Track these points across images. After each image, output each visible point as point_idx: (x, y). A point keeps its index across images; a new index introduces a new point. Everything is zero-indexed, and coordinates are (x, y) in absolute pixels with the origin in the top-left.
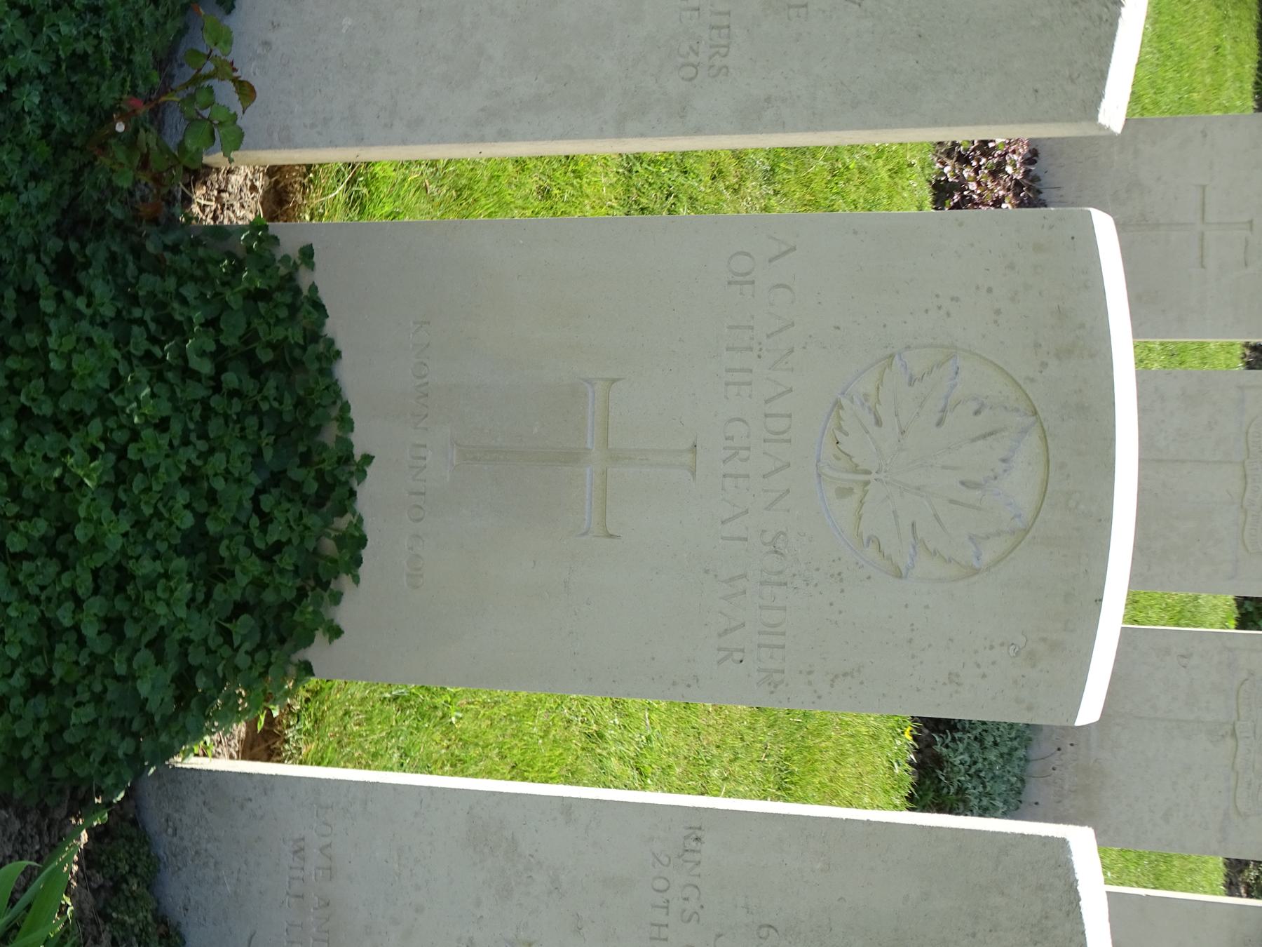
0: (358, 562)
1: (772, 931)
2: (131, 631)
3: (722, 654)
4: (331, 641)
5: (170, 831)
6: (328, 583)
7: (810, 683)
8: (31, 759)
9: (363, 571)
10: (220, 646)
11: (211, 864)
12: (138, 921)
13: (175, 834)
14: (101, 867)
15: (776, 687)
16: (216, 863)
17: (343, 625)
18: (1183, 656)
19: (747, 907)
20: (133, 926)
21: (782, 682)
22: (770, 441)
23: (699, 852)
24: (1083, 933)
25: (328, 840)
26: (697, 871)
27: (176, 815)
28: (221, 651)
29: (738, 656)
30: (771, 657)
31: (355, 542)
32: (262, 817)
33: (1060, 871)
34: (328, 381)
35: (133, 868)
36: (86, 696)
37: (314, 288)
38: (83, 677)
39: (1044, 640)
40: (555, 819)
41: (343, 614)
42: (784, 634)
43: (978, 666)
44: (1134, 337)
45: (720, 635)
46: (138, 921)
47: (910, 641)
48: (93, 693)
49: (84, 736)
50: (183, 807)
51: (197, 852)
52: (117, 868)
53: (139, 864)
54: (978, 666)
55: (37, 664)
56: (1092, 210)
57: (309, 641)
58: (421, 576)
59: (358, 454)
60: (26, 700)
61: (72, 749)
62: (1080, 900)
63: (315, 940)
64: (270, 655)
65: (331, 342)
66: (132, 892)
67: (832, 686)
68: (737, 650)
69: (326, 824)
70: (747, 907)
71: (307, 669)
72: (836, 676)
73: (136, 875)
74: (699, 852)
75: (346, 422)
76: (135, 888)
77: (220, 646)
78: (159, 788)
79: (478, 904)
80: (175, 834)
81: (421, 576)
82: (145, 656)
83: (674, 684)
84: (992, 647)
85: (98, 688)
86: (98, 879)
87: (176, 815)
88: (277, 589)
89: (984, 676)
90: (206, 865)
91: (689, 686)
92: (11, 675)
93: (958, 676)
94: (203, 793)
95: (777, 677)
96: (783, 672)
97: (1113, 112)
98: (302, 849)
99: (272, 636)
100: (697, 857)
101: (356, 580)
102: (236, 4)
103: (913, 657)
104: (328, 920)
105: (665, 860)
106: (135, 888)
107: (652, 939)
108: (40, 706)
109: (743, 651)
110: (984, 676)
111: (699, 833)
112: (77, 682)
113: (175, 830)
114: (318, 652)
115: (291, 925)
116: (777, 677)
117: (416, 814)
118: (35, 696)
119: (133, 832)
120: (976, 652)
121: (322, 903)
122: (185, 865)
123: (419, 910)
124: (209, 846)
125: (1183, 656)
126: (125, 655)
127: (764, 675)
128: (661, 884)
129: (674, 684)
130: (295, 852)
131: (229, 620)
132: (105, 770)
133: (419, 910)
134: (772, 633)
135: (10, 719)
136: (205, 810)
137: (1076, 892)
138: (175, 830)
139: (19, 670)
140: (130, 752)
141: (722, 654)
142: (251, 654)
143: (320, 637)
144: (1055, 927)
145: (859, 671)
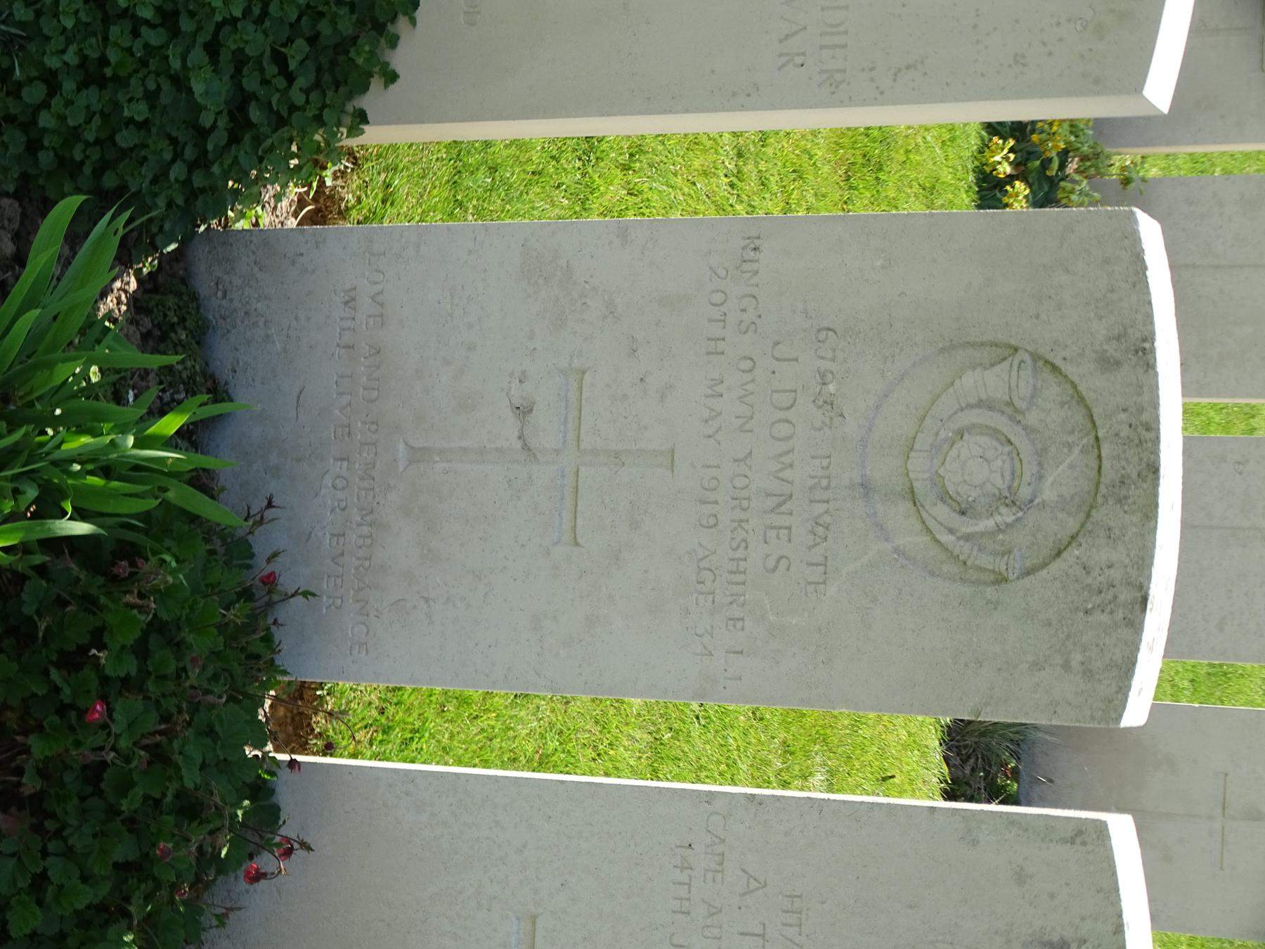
1: (831, 333)
2: (186, 25)
3: (784, 59)
4: (386, 86)
5: (220, 294)
6: (384, 25)
7: (872, 80)
8: (82, 163)
9: (420, 14)
10: (274, 76)
11: (261, 324)
12: (186, 368)
13: (224, 296)
14: (149, 312)
15: (837, 87)
16: (266, 322)
17: (399, 71)
18: (1239, 463)
19: (806, 312)
20: (180, 372)
21: (843, 81)
22: (827, 34)
23: (757, 261)
24: (1150, 303)
25: (378, 288)
26: (755, 280)
27: (226, 277)
28: (274, 81)
29: (798, 60)
30: (833, 58)
32: (313, 272)
33: (1126, 243)
35: (183, 320)
36: (139, 93)
38: (136, 71)
39: (1112, 11)
40: (611, 242)
41: (399, 59)
42: (846, 33)
43: (1044, 44)
44: (1183, 395)
45: (781, 41)
46: (186, 368)
47: (975, 26)
48: (146, 90)
49: (137, 141)
50: (233, 269)
51: (246, 313)
52: (165, 316)
53: (188, 316)
54: (1044, 44)
55: (91, 46)
56: (1139, 213)
57: (365, 88)
58: (479, 13)
60: (79, 89)
61: (125, 153)
62: (1146, 268)
63: (365, 389)
64: (325, 95)
66: (180, 341)
67: (895, 80)
68: (798, 54)
69: (377, 271)
70: (806, 312)
72: (899, 70)
73: (185, 328)
74: (757, 261)
76: (183, 337)
77: (274, 76)
78: (210, 252)
79: (531, 335)
80: (224, 296)
81: (479, 13)
82: (198, 56)
83: (734, 94)
84: (1059, 24)
85: (152, 86)
86: (147, 323)
87: (226, 277)
88: (334, 23)
89: (1050, 54)
90: (255, 324)
91: (749, 95)
92: (63, 52)
93: (1023, 56)
94: (254, 253)
95: (838, 77)
96: (844, 71)
97: (1160, 89)
98: (353, 299)
99: (327, 78)
100: (755, 266)
101: (413, 22)
103: (978, 42)
104: (378, 367)
105: (722, 273)
106: (183, 337)
107: (708, 353)
108: (91, 97)
109: (804, 54)
110: (1050, 54)
111: (757, 242)
112: (130, 75)
113: (225, 293)
114: (373, 99)
115: (342, 377)
116: (838, 77)
117: (470, 252)
118: (87, 88)
119: (183, 289)
120: (1042, 30)
121: (373, 351)
122: (235, 327)
123: (471, 348)
124: (259, 305)
125: (1239, 463)
126: (179, 49)
127: (825, 76)
128: (718, 298)
129: (734, 94)
130: (346, 303)
131: (284, 45)
132: (156, 189)
133: (471, 348)
134: (833, 34)
135: (62, 102)
136: (256, 269)
137: (1143, 261)
138: (225, 293)
139: (73, 48)
140: (182, 178)
141: (784, 59)
142: (307, 92)
143: (376, 83)
144: (1121, 300)
145: (922, 62)
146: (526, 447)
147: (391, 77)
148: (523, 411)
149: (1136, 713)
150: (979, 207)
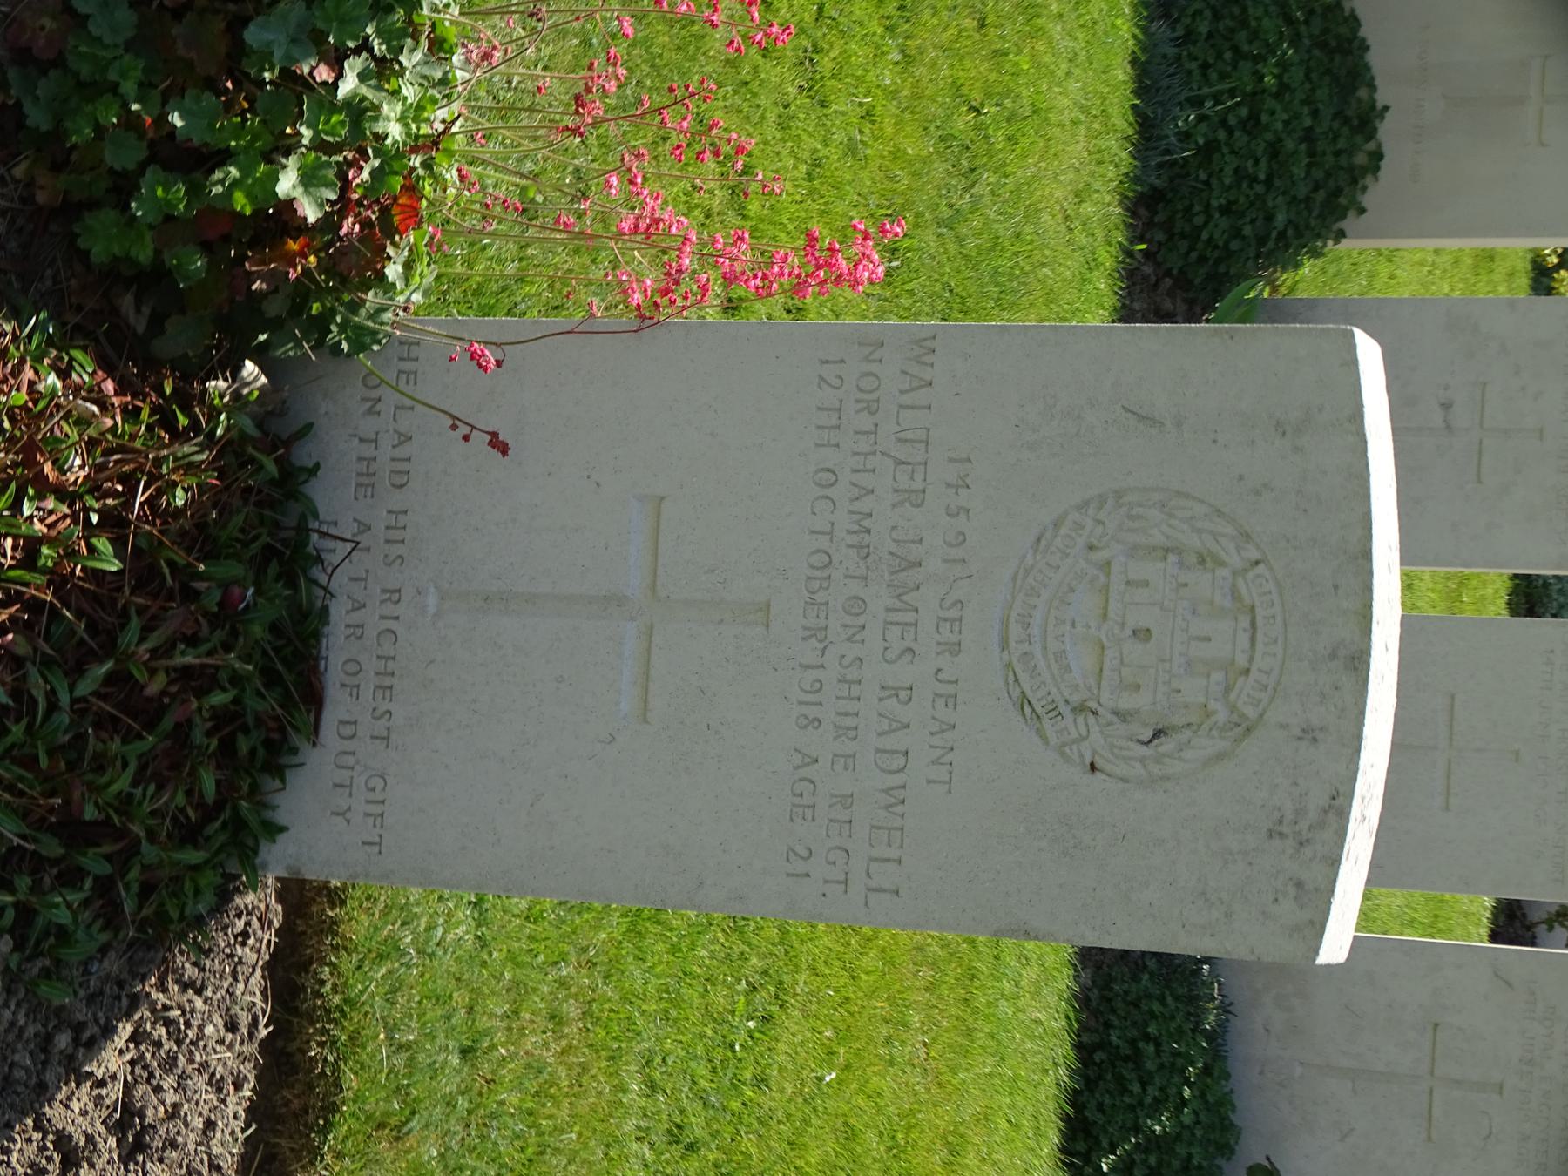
0: (1378, 168)
9: (1381, 174)
31: (1378, 156)
34: (1371, 146)
37: (1353, 10)
41: (1367, 200)
57: (1343, 217)
59: (1379, 105)
65: (1364, 40)
71: (1341, 234)
75: (1372, 87)
101: (1377, 179)
102: (1340, 56)
143: (1351, 214)
146: (1448, 427)
147: (1362, 211)
148: (1446, 406)
149: (1335, 947)
150: (1126, 314)
